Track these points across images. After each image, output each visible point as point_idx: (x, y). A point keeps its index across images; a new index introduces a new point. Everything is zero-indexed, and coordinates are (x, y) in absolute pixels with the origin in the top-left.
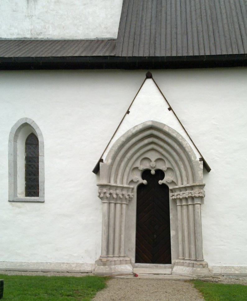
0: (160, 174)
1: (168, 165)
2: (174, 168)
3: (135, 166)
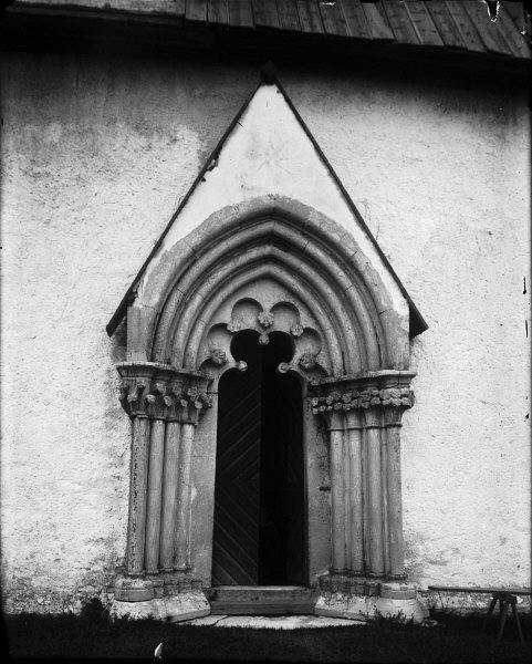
0: (283, 345)
1: (306, 321)
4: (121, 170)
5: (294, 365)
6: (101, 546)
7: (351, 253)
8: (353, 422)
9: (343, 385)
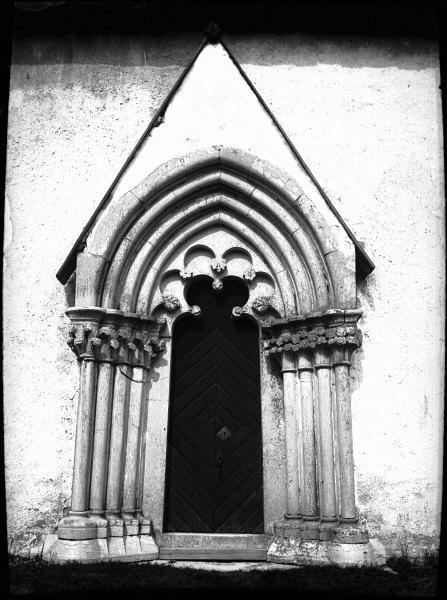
0: (238, 288)
1: (259, 266)
2: (274, 274)
3: (171, 267)
4: (77, 130)
5: (248, 308)
6: (51, 488)
7: (295, 197)
8: (303, 362)
9: (294, 325)
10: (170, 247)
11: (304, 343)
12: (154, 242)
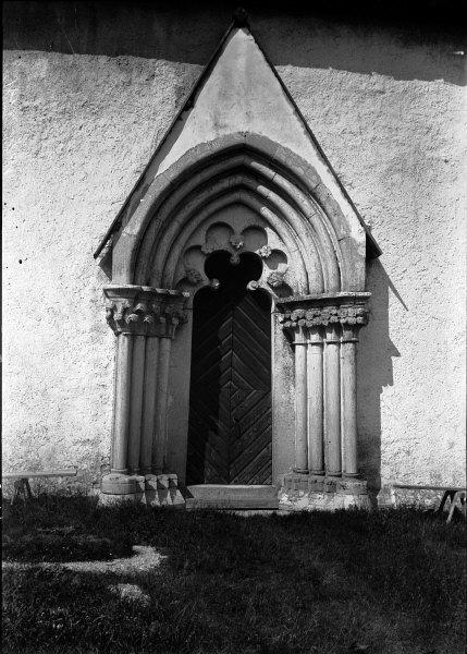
7: (314, 185)
10: (194, 224)
11: (316, 321)
12: (181, 221)
